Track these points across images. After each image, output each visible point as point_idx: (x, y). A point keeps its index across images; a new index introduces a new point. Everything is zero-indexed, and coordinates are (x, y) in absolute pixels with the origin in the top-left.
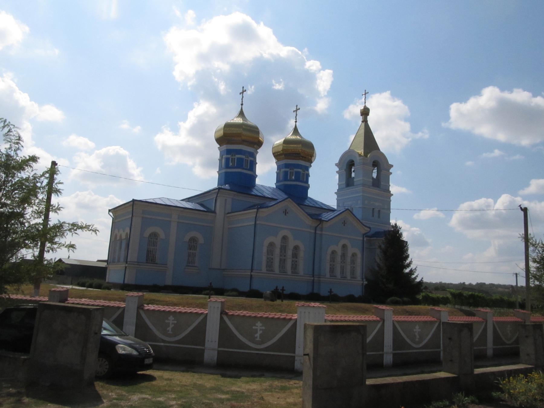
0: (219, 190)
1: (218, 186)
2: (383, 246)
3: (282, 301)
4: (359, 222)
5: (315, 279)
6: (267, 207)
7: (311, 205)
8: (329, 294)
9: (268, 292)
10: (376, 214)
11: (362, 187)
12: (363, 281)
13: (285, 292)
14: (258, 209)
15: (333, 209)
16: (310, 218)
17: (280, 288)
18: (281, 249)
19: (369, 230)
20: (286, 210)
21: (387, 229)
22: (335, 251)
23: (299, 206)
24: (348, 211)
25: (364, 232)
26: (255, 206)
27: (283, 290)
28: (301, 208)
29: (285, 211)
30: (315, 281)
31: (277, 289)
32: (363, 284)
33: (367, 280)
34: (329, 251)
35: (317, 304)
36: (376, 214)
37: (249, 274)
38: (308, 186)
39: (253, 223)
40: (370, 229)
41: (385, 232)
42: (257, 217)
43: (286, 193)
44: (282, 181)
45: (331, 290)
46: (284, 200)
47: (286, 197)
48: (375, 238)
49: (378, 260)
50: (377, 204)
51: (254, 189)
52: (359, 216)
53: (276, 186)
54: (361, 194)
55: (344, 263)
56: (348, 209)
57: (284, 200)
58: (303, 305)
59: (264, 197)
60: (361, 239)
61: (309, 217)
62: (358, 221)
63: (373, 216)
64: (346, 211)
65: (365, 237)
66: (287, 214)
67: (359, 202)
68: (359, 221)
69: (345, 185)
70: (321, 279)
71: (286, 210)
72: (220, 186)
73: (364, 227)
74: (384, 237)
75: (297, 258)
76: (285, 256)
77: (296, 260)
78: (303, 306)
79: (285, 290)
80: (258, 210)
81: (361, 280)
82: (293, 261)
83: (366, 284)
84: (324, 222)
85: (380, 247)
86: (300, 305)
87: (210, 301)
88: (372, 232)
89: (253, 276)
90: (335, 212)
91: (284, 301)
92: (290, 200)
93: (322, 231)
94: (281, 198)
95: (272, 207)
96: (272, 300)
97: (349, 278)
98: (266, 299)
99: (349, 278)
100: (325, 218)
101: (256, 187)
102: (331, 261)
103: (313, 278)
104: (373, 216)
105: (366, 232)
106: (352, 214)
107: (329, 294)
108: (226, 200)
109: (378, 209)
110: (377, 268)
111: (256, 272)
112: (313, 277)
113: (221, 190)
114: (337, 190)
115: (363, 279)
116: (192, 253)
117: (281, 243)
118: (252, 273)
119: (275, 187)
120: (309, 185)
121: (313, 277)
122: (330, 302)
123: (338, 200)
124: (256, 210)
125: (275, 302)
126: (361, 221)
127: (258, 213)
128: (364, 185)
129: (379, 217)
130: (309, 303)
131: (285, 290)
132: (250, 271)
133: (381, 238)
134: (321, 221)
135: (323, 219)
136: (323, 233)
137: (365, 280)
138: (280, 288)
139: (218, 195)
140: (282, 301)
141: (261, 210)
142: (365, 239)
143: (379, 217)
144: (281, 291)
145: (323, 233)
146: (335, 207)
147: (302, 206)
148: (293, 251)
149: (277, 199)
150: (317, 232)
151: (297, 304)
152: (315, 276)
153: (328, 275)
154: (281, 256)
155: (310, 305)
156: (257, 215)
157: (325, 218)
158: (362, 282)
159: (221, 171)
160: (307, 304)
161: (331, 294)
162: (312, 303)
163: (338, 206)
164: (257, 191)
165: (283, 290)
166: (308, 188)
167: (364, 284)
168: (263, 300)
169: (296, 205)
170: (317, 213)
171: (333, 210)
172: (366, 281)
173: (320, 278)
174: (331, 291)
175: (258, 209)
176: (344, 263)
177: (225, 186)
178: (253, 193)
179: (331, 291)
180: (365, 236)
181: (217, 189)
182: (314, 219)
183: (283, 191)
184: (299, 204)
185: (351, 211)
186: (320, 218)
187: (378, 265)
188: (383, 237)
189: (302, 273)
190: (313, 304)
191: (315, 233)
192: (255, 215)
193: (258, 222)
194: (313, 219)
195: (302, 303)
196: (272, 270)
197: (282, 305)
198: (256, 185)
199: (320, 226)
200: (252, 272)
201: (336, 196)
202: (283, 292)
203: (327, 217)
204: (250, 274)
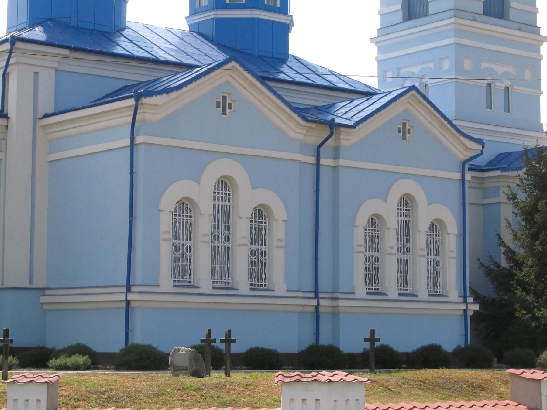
0: (12, 45)
1: (8, 34)
2: (522, 196)
3: (227, 374)
4: (449, 126)
5: (322, 302)
6: (167, 91)
7: (299, 78)
8: (367, 345)
9: (183, 349)
10: (498, 98)
11: (453, 20)
12: (465, 302)
13: (235, 349)
14: (138, 98)
15: (370, 91)
16: (299, 120)
17: (218, 335)
18: (215, 219)
19: (479, 147)
20: (224, 98)
21: (531, 144)
22: (377, 216)
23: (263, 84)
24: (413, 92)
25: (464, 155)
26: (126, 88)
27: (228, 340)
28: (270, 89)
29: (221, 100)
30: (321, 309)
31: (209, 339)
32: (465, 311)
33: (477, 298)
34: (362, 220)
35: (340, 375)
36: (498, 98)
37: (122, 297)
38: (288, 22)
39: (127, 142)
40: (483, 147)
41: (527, 151)
42: (136, 125)
43: (221, 47)
44: (207, 10)
45: (372, 332)
46: (218, 67)
47: (220, 56)
48: (498, 173)
49: (508, 238)
50: (500, 69)
51: (122, 39)
52: (449, 110)
53: (190, 26)
54: (451, 40)
55: (408, 250)
56: (413, 88)
57: (218, 67)
58: (297, 377)
59: (156, 61)
60: (458, 176)
61: (295, 116)
62: (446, 123)
63: (489, 105)
64: (408, 95)
65: (469, 169)
66: (228, 111)
67: (446, 65)
68: (449, 122)
69: (400, 14)
70: (341, 303)
71: (224, 98)
72: (16, 34)
73: (462, 138)
74: (524, 170)
75: (264, 243)
76: (228, 239)
77: (263, 248)
78: (298, 381)
79: (234, 341)
80: (137, 100)
81: (461, 300)
82: (252, 253)
83: (475, 311)
84: (342, 129)
85: (513, 198)
86: (287, 380)
87: (13, 382)
88: (490, 154)
89: (133, 304)
90: (375, 98)
91: (231, 374)
92: (237, 66)
93: (336, 157)
94: (208, 61)
95: (180, 92)
96: (197, 374)
97: (423, 294)
98: (177, 370)
99: (423, 294)
100: (344, 116)
101: (126, 32)
102: (367, 249)
103: (314, 302)
104: (489, 105)
105: (472, 154)
106: (425, 103)
107: (367, 345)
108: (36, 73)
109: (486, 82)
110: (504, 264)
111: (140, 292)
112: (316, 297)
113: (19, 45)
114: (376, 32)
115: (465, 297)
116: (222, 205)
117: (215, 200)
118: (130, 297)
119: (187, 29)
120: (292, 16)
121: (316, 297)
122: (372, 371)
123: (380, 62)
124: (131, 102)
125: (206, 379)
126: (454, 122)
127: (139, 111)
128: (458, 12)
129: (507, 109)
130: (314, 374)
131: (234, 341)
132: (124, 290)
133: (515, 173)
134: (333, 126)
135: (338, 120)
136: (342, 162)
137: (470, 300)
138: (218, 335)
139: (12, 61)
140: (227, 374)
141: (144, 100)
142: (468, 176)
143: (507, 109)
144: (222, 346)
145: (342, 162)
146: (374, 83)
147: (270, 84)
148: (251, 221)
149: (198, 66)
150: (323, 161)
151: (280, 378)
152: (320, 295)
153: (361, 291)
154: (216, 238)
155: (319, 377)
156: (138, 117)
157: (344, 116)
158: (463, 307)
159: (209, 14)
160: (310, 375)
161: (372, 345)
162: (323, 372)
163: (382, 77)
164: (131, 44)
165: (228, 340)
166: (286, 28)
167: (470, 313)
168: (168, 373)
169: (254, 80)
170: (320, 102)
171: (368, 94)
172: (475, 300)
173: (336, 299)
174: (372, 339)
175: (138, 98)
176: (408, 250)
177: (32, 32)
178: (119, 50)
179: (372, 339)
180: (467, 166)
181: (6, 40)
182: (312, 121)
183: (212, 41)
184: (263, 80)
185: (423, 93)
186: (330, 117)
187: (510, 254)
188: (520, 169)
189: (280, 289)
190: (326, 375)
191: (318, 164)
192: (130, 119)
193: (139, 139)
194: (307, 120)
195: (292, 374)
196: (190, 282)
197: (228, 386)
198: (128, 24)
199: (330, 142)
200: (128, 290)
201: (374, 50)
202: (228, 347)
203: (348, 116)
204: (124, 299)
